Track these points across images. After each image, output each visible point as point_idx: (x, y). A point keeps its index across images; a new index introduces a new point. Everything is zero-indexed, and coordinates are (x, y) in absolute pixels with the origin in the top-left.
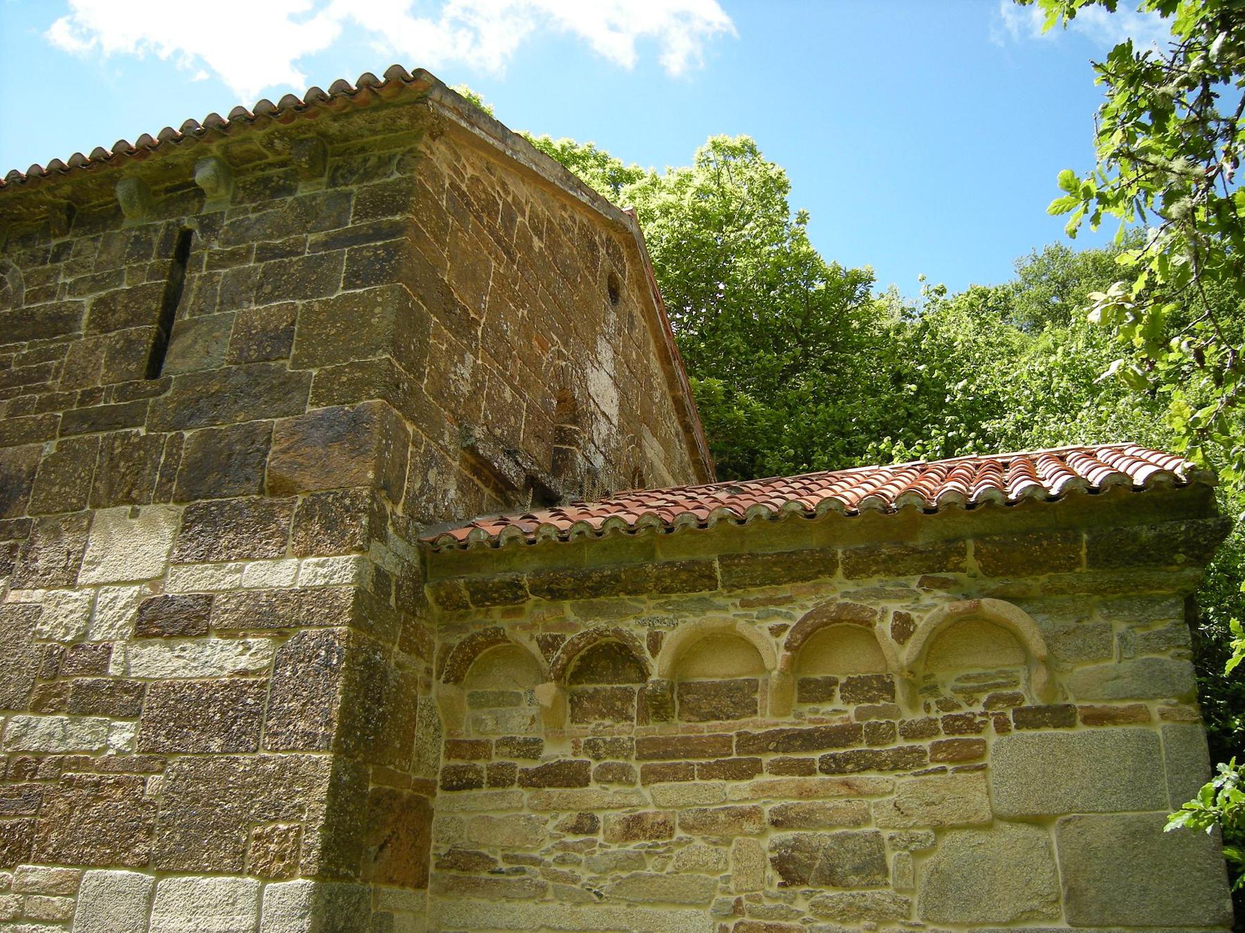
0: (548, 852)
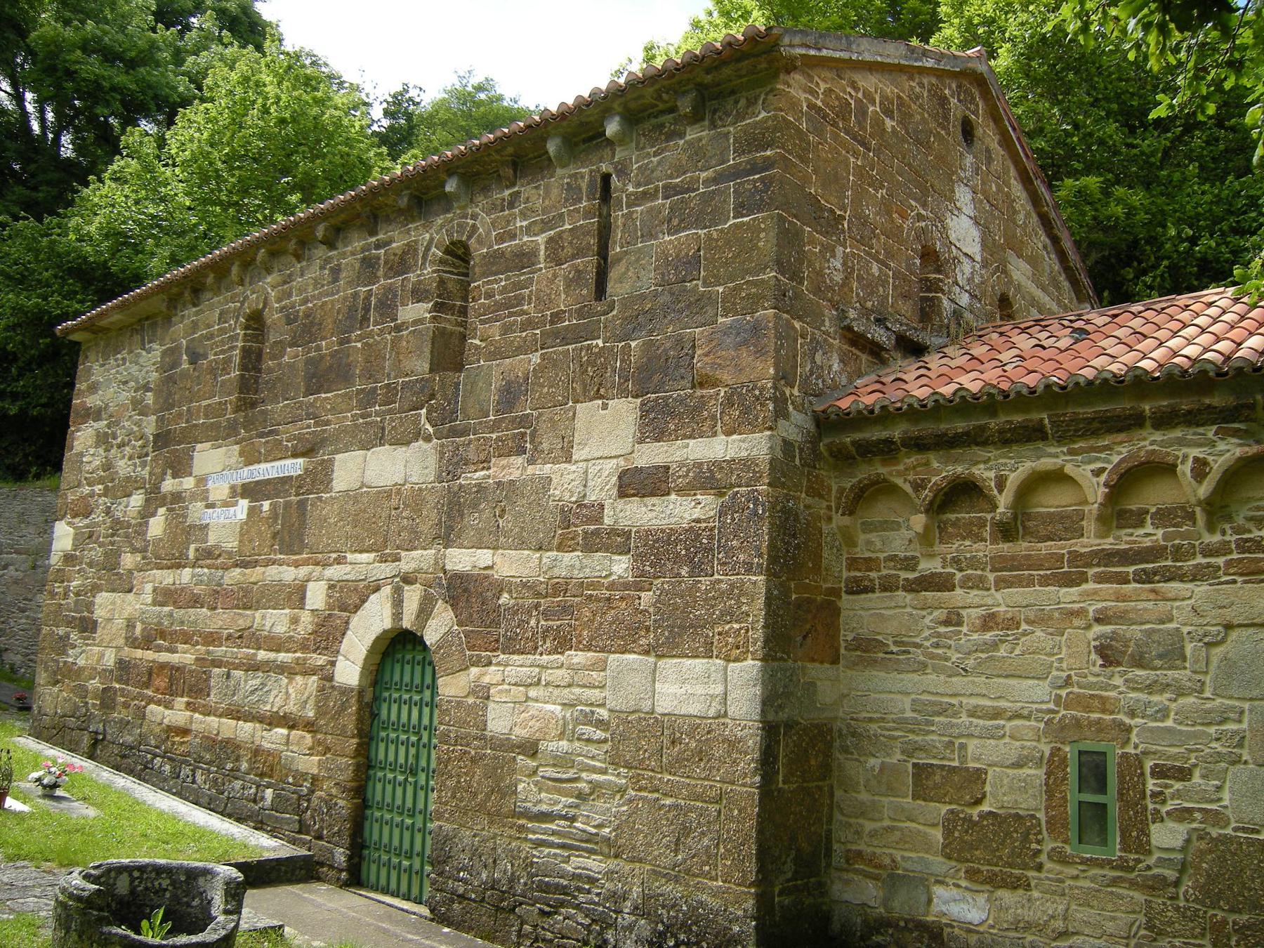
0: (926, 639)
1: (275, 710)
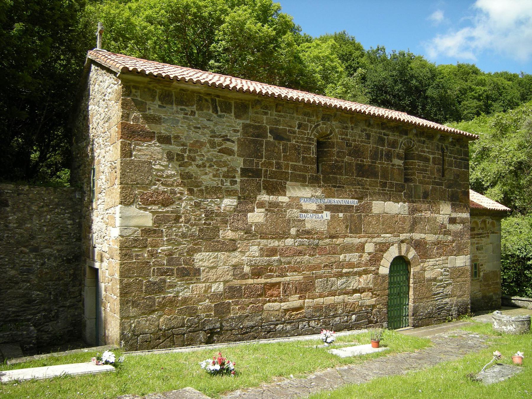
1: (354, 288)
